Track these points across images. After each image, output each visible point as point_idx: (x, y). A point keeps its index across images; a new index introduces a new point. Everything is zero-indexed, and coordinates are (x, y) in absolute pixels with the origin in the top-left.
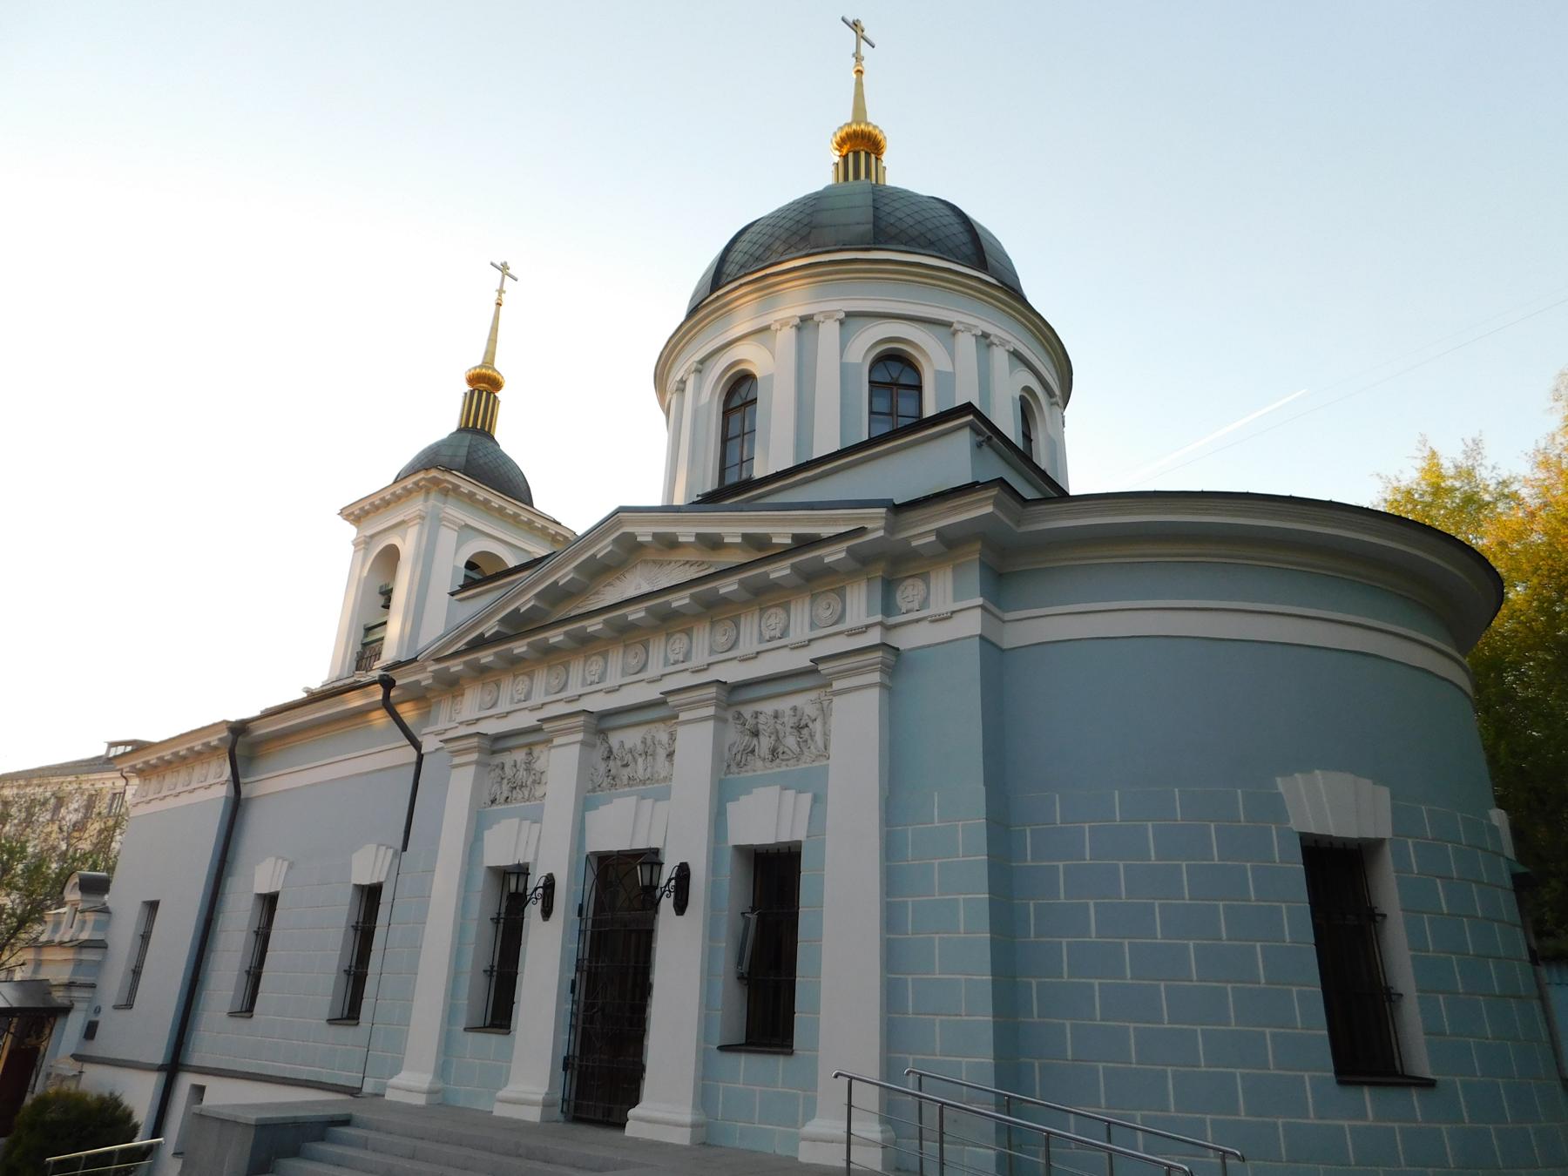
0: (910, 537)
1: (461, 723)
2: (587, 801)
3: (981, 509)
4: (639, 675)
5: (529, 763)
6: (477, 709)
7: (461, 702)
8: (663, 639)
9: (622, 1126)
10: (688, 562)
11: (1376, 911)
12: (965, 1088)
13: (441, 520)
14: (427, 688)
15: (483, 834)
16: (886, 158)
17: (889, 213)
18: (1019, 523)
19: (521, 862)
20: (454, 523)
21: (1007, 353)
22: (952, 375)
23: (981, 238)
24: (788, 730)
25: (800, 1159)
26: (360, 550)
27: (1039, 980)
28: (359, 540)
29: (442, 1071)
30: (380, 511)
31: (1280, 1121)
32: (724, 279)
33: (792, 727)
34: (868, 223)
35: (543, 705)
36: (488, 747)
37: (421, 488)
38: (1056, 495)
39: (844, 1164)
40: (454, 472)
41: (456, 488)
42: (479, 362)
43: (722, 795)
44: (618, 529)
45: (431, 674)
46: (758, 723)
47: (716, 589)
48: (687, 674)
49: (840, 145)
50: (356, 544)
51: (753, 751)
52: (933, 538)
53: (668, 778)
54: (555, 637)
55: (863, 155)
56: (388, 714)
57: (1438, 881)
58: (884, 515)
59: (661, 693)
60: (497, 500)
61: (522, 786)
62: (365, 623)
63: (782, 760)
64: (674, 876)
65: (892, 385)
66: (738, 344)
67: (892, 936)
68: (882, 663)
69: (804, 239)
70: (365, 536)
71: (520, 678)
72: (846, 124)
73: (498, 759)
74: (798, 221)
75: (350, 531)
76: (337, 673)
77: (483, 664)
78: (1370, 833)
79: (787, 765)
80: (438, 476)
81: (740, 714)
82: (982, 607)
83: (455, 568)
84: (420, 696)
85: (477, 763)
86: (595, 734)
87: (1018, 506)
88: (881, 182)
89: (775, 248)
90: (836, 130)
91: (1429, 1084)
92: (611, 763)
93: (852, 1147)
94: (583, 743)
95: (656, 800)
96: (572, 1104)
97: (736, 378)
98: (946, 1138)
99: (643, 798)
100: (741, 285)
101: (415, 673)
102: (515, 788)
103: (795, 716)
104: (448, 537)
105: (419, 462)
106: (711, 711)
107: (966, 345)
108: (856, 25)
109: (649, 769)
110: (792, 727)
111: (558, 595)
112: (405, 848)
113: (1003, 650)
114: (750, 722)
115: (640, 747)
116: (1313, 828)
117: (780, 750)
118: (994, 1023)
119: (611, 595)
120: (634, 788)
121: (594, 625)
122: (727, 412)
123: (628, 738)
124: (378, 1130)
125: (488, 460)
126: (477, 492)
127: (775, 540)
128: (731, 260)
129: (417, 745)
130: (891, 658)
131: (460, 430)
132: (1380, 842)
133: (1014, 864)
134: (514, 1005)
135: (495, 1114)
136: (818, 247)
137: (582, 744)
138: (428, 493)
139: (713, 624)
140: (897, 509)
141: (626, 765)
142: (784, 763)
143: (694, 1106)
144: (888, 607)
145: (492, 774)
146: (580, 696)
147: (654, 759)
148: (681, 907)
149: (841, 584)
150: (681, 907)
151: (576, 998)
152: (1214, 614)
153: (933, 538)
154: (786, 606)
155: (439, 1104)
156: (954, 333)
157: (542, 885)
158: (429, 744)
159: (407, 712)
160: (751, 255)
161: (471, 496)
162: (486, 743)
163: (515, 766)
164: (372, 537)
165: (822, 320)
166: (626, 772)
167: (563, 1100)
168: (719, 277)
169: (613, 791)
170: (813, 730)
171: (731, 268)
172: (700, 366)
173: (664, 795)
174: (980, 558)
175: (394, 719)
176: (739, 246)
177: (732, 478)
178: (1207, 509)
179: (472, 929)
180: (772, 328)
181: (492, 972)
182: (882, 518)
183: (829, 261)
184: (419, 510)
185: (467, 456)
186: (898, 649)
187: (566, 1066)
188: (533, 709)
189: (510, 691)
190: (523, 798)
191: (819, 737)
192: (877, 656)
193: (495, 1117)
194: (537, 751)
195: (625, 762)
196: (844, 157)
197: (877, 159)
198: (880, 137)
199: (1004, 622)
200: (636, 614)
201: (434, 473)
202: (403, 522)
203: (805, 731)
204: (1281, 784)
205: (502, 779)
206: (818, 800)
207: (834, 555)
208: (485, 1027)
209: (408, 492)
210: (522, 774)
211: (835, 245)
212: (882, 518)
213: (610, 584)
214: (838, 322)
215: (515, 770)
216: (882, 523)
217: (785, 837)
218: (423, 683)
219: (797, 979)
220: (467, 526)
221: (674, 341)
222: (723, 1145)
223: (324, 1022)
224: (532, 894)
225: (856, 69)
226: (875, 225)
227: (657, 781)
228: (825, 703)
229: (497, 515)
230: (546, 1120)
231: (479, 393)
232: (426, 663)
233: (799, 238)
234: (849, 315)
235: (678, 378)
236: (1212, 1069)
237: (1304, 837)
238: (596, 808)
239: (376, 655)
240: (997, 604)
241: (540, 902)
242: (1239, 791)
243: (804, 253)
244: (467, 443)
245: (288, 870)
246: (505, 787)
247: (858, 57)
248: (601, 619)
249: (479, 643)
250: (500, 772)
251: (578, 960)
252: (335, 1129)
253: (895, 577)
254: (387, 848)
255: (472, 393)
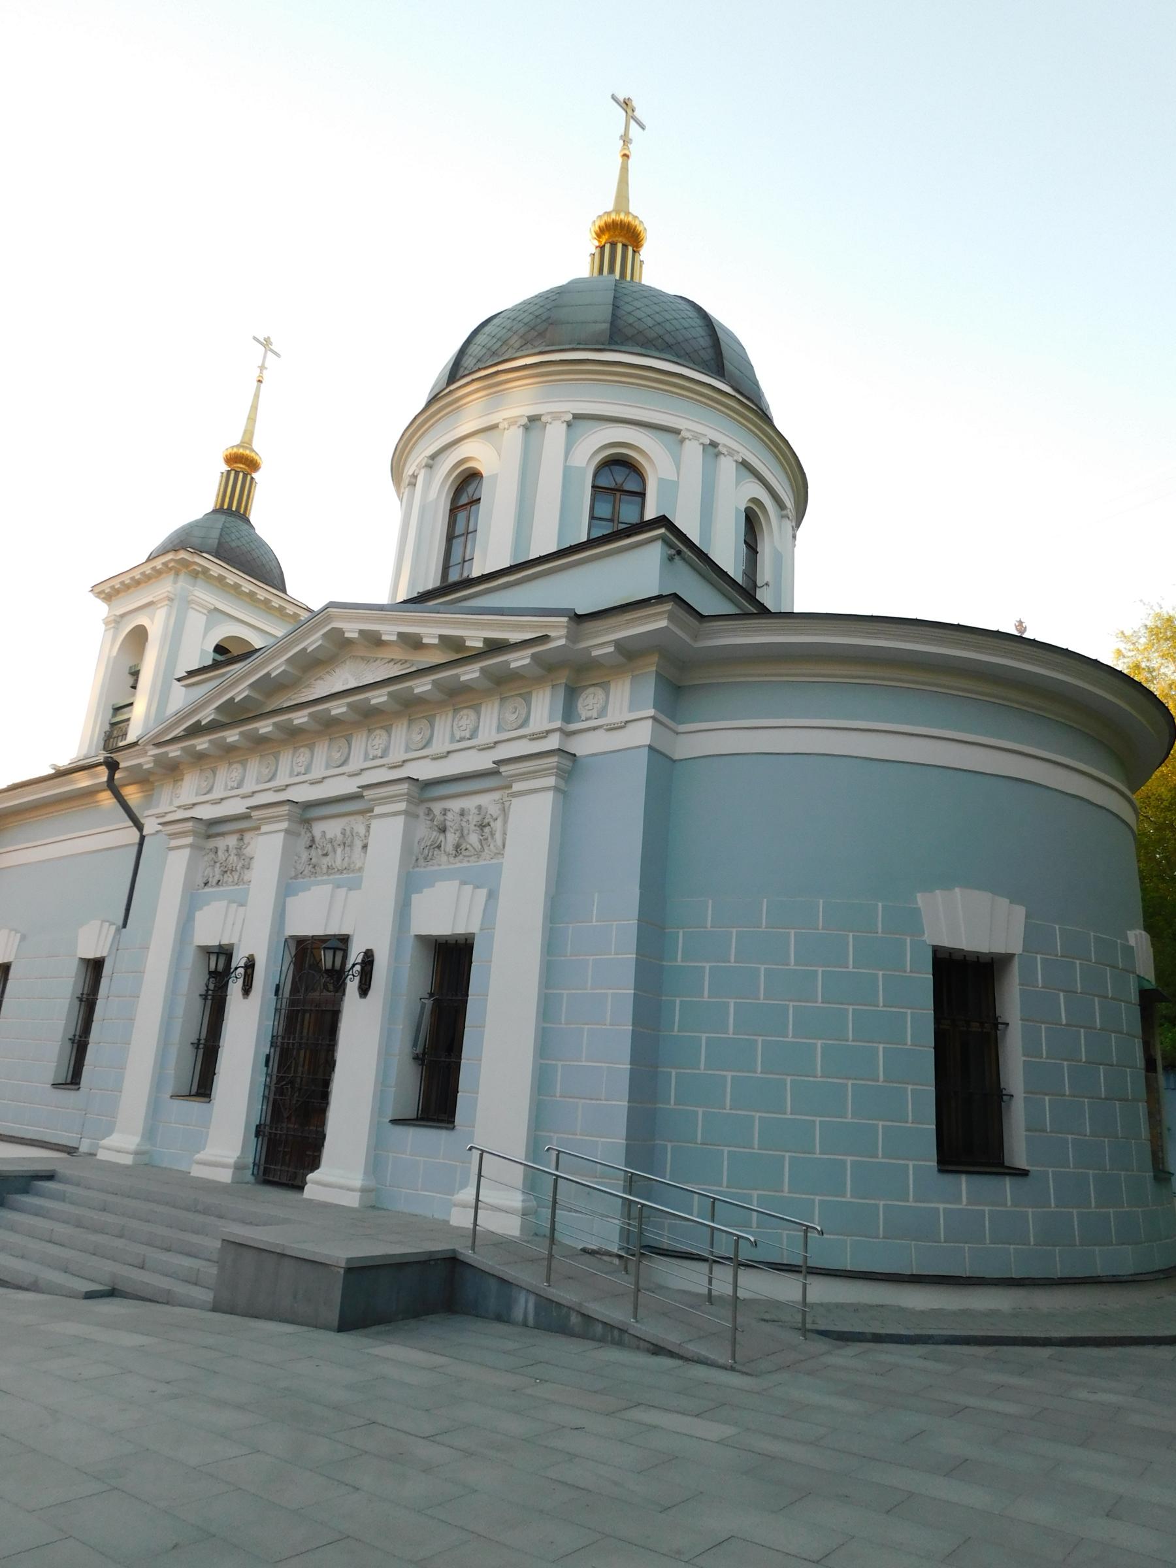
0: (591, 646)
1: (179, 807)
2: (287, 888)
3: (656, 622)
4: (340, 768)
5: (240, 849)
6: (194, 794)
7: (181, 786)
8: (365, 734)
9: (301, 1188)
10: (392, 660)
11: (1000, 1020)
12: (599, 1165)
13: (189, 602)
14: (149, 772)
15: (194, 914)
16: (645, 253)
17: (629, 313)
18: (695, 637)
19: (222, 943)
20: (204, 607)
21: (734, 464)
22: (676, 484)
23: (722, 343)
24: (472, 827)
25: (451, 1223)
26: (110, 629)
27: (679, 1071)
28: (109, 619)
29: (150, 1133)
30: (131, 590)
31: (882, 1203)
32: (461, 372)
33: (475, 825)
34: (604, 322)
35: (254, 793)
36: (203, 831)
37: (171, 569)
38: (755, 612)
39: (471, 1226)
40: (204, 555)
41: (205, 571)
42: (237, 440)
43: (408, 886)
44: (326, 625)
45: (152, 758)
46: (445, 820)
47: (411, 688)
48: (383, 770)
49: (599, 235)
50: (106, 622)
51: (439, 847)
52: (611, 649)
53: (361, 869)
54: (265, 727)
55: (620, 246)
56: (112, 796)
57: (1062, 994)
58: (566, 624)
59: (359, 787)
60: (247, 585)
61: (232, 870)
62: (114, 702)
63: (465, 856)
64: (359, 960)
65: (616, 491)
66: (465, 441)
67: (548, 1025)
68: (558, 768)
69: (541, 335)
70: (115, 615)
71: (235, 766)
72: (606, 213)
73: (212, 843)
74: (537, 317)
75: (102, 609)
76: (84, 752)
77: (229, 743)
78: (999, 948)
79: (468, 861)
80: (186, 557)
81: (430, 810)
82: (654, 718)
83: (203, 651)
84: (144, 779)
85: (191, 846)
86: (301, 823)
87: (697, 623)
88: (636, 279)
89: (511, 343)
90: (595, 219)
91: (1024, 1173)
92: (313, 852)
93: (479, 1211)
94: (287, 831)
95: (350, 889)
96: (262, 1168)
97: (464, 476)
98: (557, 1206)
99: (339, 887)
100: (473, 381)
101: (138, 756)
102: (226, 872)
103: (479, 814)
104: (196, 620)
105: (171, 543)
106: (402, 806)
107: (693, 452)
108: (627, 104)
109: (346, 859)
110: (475, 825)
111: (270, 686)
112: (124, 926)
113: (674, 761)
114: (439, 818)
115: (340, 837)
116: (946, 942)
117: (463, 846)
118: (630, 1108)
119: (321, 689)
120: (331, 877)
121: (300, 718)
122: (454, 510)
123: (329, 829)
124: (78, 1185)
125: (240, 544)
126: (226, 575)
127: (468, 643)
128: (469, 353)
129: (139, 826)
130: (567, 763)
131: (215, 511)
132: (1007, 958)
133: (665, 963)
134: (215, 1077)
135: (192, 1174)
136: (552, 345)
137: (286, 833)
138: (178, 575)
139: (411, 721)
140: (579, 618)
141: (326, 855)
142: (466, 859)
143: (365, 1173)
144: (569, 713)
145: (206, 858)
146: (287, 786)
147: (352, 850)
148: (364, 990)
149: (528, 690)
150: (364, 990)
151: (270, 1071)
152: (873, 735)
153: (611, 649)
154: (476, 708)
155: (146, 1164)
156: (682, 441)
157: (360, 961)
158: (150, 826)
159: (132, 794)
160: (489, 349)
161: (221, 579)
162: (201, 828)
163: (227, 851)
164: (123, 616)
165: (550, 420)
166: (326, 861)
167: (254, 1164)
168: (455, 372)
169: (313, 879)
170: (494, 829)
171: (468, 362)
172: (431, 462)
173: (355, 885)
174: (656, 671)
175: (119, 801)
176: (481, 339)
177: (454, 577)
178: (874, 633)
179: (182, 1002)
180: (501, 426)
181: (198, 1044)
182: (563, 627)
183: (561, 360)
184: (168, 592)
185: (219, 539)
186: (575, 755)
187: (258, 1133)
188: (244, 797)
189: (225, 777)
190: (233, 882)
191: (498, 836)
192: (553, 760)
193: (193, 1177)
194: (248, 836)
195: (325, 852)
196: (601, 248)
197: (634, 251)
198: (640, 228)
199: (677, 733)
200: (338, 708)
201: (182, 555)
202: (151, 604)
203: (487, 830)
204: (921, 899)
205: (215, 862)
206: (492, 895)
207: (519, 660)
208: (190, 1096)
209: (158, 573)
210: (233, 858)
211: (570, 344)
212: (563, 627)
213: (320, 678)
214: (565, 424)
215: (227, 855)
216: (563, 632)
217: (461, 929)
218: (145, 767)
219: (463, 1061)
220: (216, 609)
221: (411, 431)
222: (389, 1208)
223: (49, 1086)
224: (349, 971)
225: (622, 154)
226: (612, 323)
227: (353, 871)
228: (507, 804)
229: (248, 600)
230: (236, 1181)
231: (235, 474)
232: (147, 748)
233: (536, 334)
234: (577, 417)
235: (410, 473)
236: (826, 1156)
237: (936, 950)
238: (296, 894)
239: (123, 735)
240: (673, 718)
241: (357, 979)
242: (880, 904)
243: (537, 350)
244: (219, 525)
245: (20, 942)
246: (217, 870)
247: (626, 140)
248: (306, 712)
249: (196, 730)
250: (213, 856)
251: (273, 1037)
252: (35, 1182)
253: (576, 686)
254: (110, 925)
255: (229, 472)
